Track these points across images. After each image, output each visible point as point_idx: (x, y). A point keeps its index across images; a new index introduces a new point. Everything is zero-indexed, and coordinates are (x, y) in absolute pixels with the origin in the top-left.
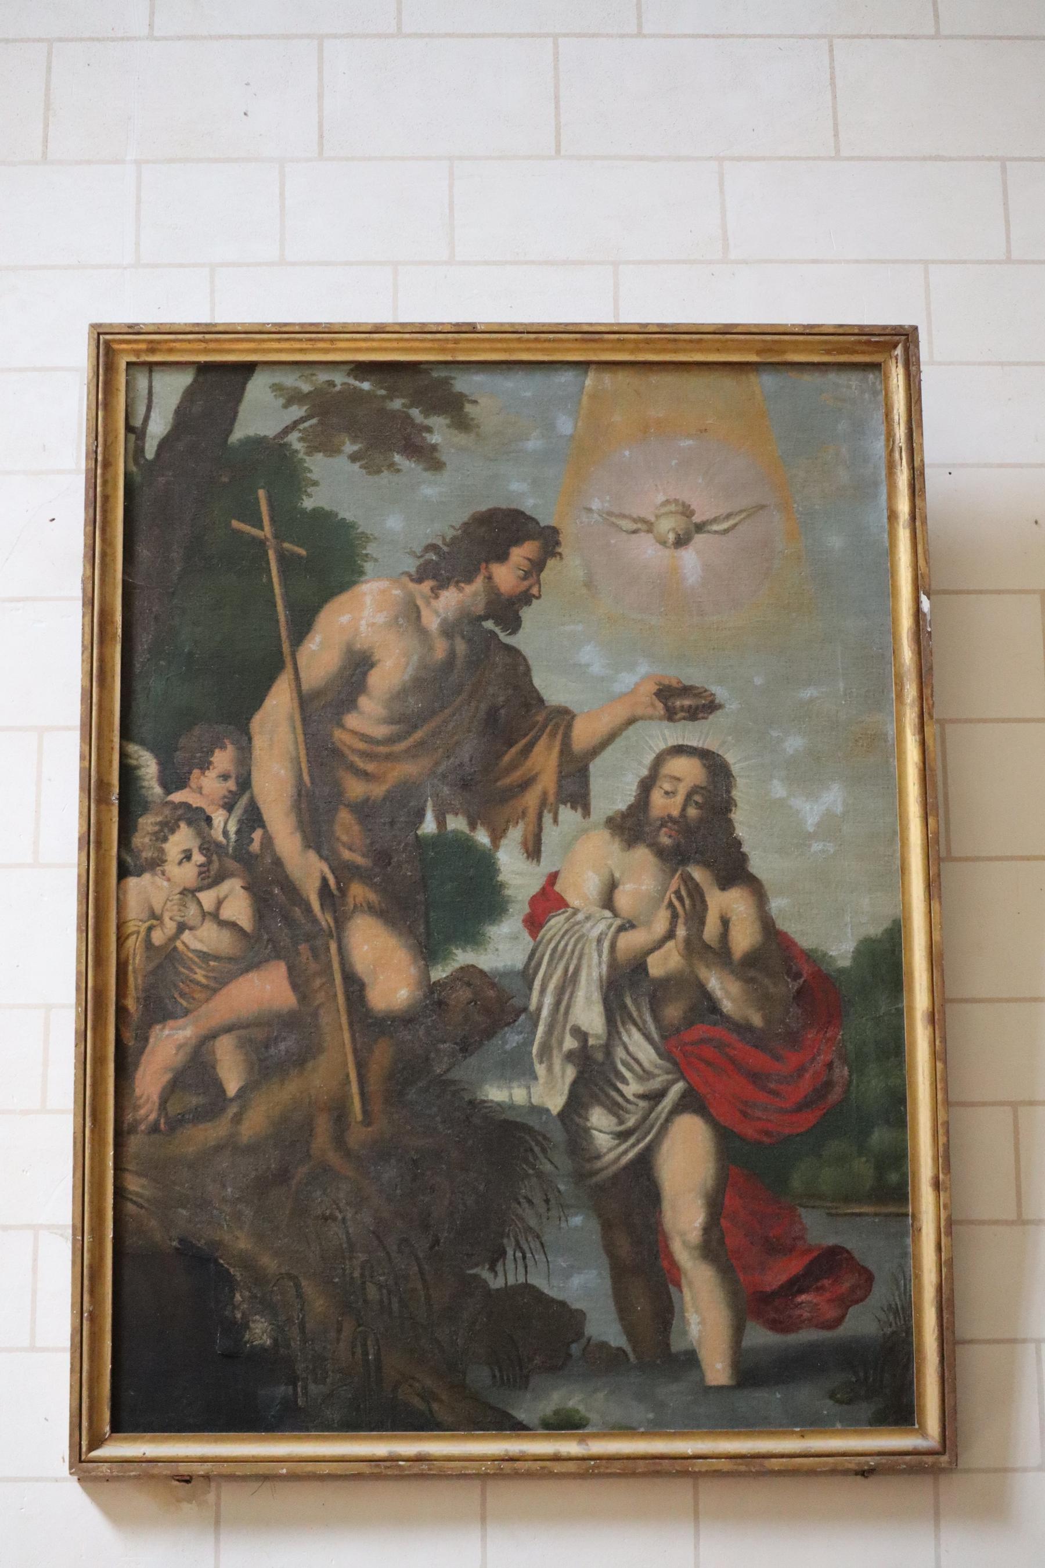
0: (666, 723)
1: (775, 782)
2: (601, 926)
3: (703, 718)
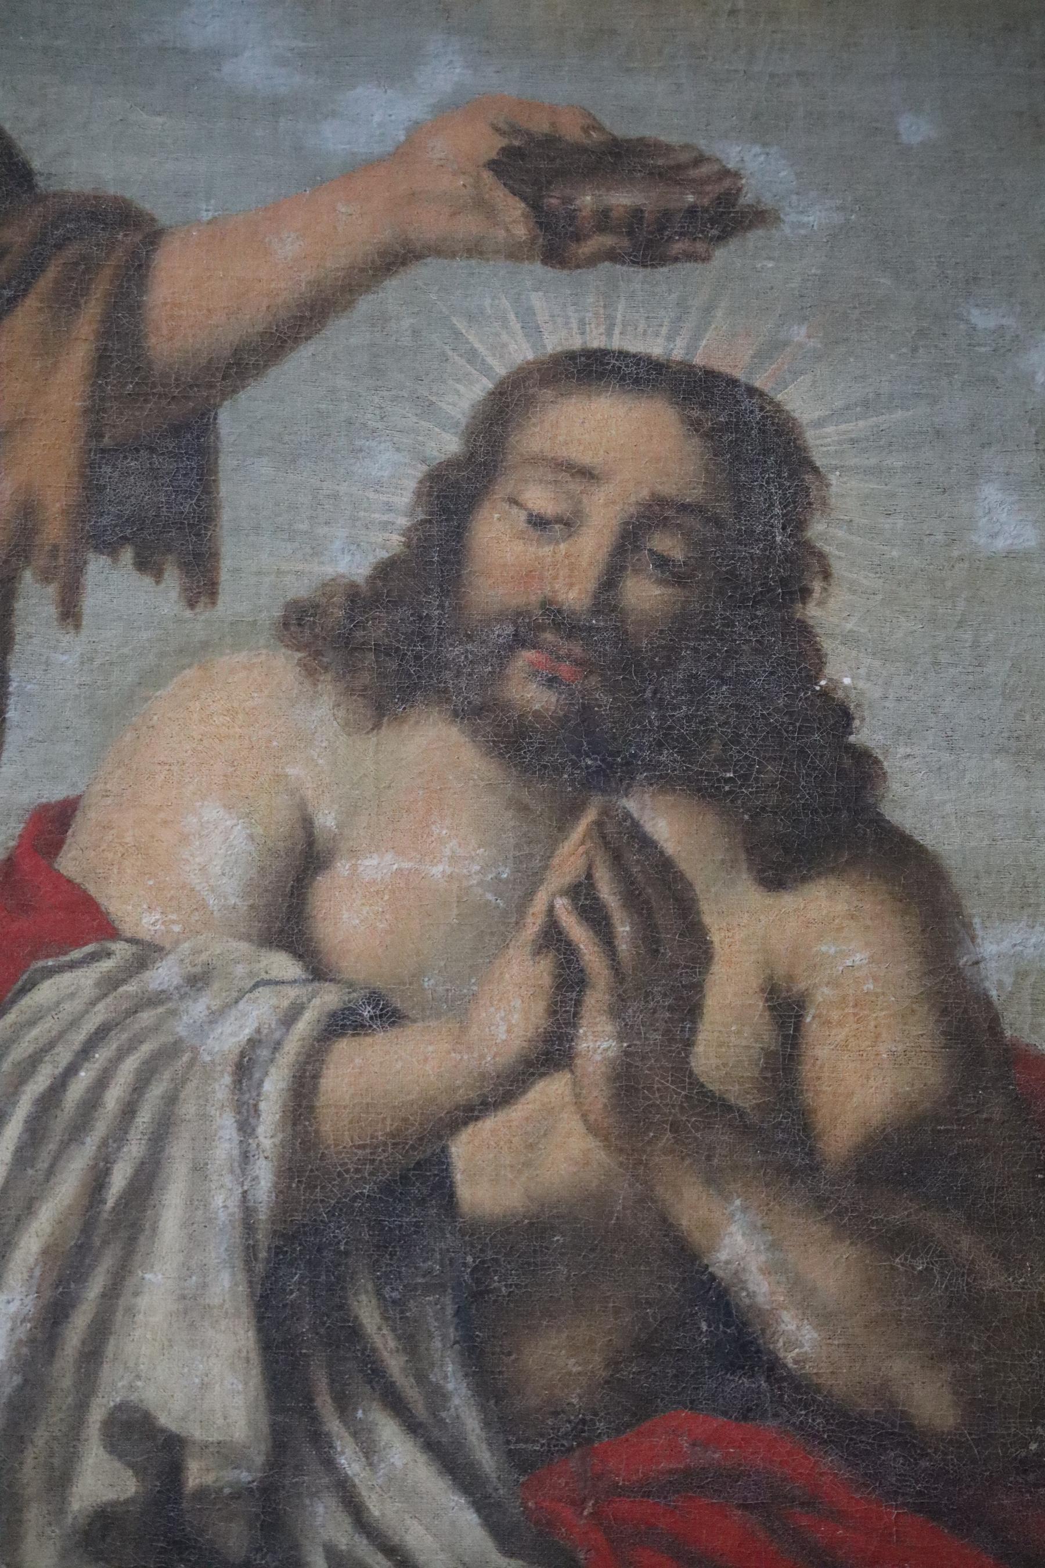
0: (538, 268)
1: (991, 493)
2: (256, 1013)
3: (691, 257)
